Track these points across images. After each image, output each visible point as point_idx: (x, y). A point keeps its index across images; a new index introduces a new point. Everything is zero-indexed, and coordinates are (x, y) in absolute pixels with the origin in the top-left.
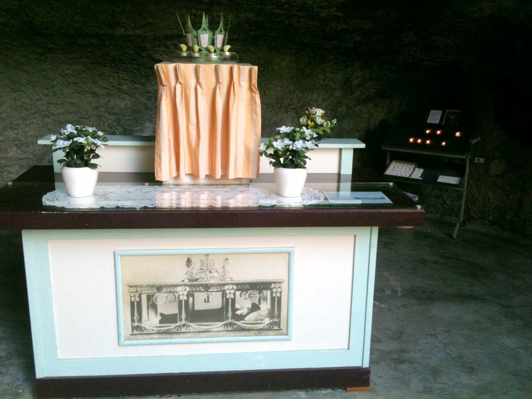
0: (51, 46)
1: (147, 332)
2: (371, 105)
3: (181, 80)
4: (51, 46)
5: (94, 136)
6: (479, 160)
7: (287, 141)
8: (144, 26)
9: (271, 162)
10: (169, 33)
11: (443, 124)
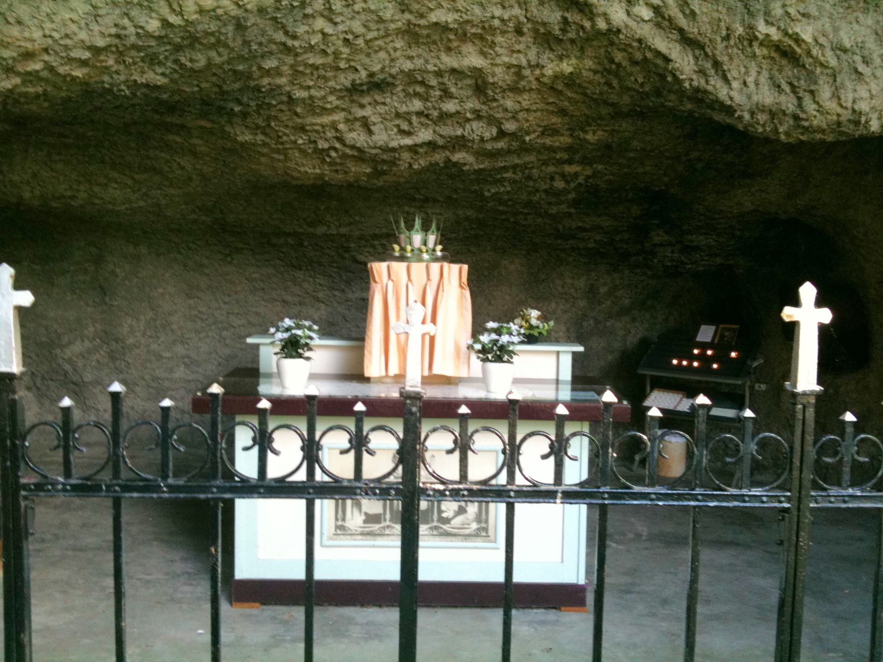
0: (240, 245)
1: (351, 532)
2: (627, 318)
3: (392, 277)
4: (240, 245)
5: (310, 329)
6: (760, 387)
7: (494, 336)
8: (350, 224)
9: (478, 358)
10: (377, 231)
11: (716, 341)
